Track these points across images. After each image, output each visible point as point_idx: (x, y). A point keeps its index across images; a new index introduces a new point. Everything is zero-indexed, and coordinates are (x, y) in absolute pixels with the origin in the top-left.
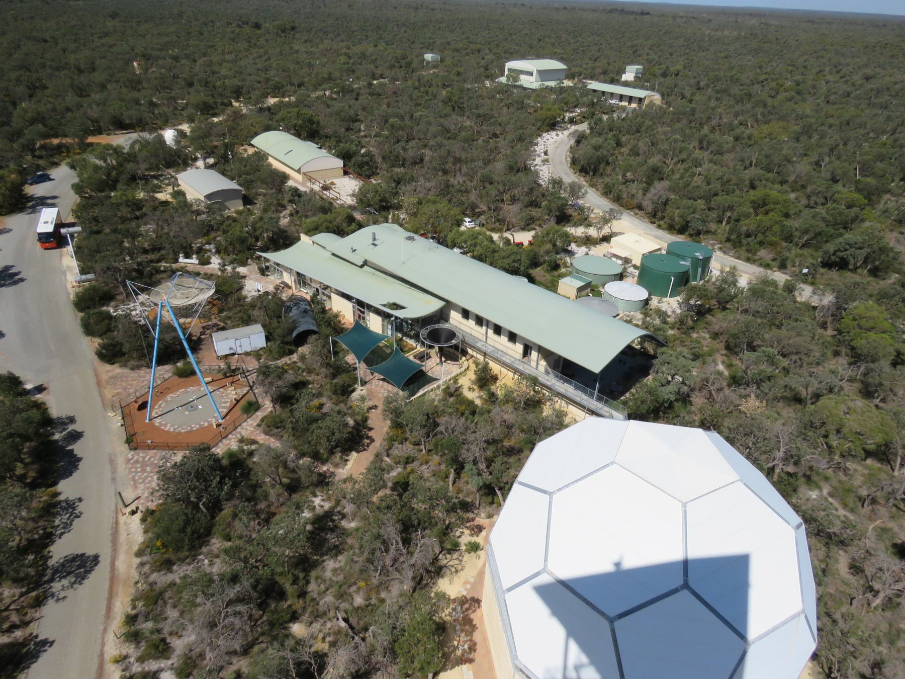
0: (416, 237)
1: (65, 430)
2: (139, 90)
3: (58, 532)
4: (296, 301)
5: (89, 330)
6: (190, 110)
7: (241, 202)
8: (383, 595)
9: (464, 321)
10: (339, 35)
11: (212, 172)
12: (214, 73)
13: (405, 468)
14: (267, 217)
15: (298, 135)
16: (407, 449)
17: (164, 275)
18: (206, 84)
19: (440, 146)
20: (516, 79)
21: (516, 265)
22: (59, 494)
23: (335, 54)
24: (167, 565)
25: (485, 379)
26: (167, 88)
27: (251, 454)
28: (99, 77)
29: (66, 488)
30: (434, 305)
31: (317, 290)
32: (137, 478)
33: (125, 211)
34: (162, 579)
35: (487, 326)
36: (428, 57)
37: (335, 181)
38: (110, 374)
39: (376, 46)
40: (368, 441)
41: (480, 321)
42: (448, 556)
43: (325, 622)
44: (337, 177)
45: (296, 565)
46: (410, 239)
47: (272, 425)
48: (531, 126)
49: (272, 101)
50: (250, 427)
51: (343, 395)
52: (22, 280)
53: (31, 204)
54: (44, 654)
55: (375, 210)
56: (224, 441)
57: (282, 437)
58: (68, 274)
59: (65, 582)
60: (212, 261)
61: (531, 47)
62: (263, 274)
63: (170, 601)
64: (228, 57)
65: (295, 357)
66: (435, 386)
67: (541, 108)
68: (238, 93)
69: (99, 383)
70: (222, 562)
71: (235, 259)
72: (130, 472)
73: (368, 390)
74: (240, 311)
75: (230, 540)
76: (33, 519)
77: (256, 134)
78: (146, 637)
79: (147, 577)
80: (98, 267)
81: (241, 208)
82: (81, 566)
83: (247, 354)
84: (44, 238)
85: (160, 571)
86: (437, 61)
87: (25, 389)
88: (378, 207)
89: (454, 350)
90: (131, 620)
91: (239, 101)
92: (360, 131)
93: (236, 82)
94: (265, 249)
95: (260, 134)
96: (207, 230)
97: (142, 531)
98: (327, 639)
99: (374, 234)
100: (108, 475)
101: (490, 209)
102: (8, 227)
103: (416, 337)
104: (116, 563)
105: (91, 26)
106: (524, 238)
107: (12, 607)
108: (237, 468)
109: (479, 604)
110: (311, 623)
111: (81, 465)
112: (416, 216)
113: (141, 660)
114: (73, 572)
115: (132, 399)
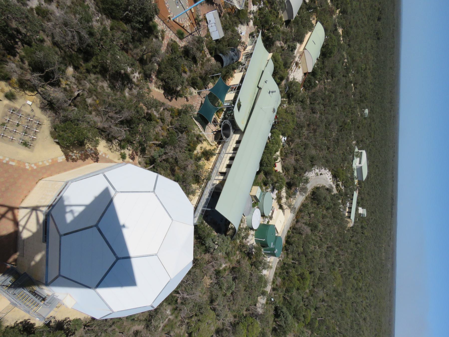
0: (275, 113)
4: (238, 54)
7: (287, 19)
9: (235, 142)
10: (376, 64)
13: (159, 118)
14: (280, 35)
15: (323, 47)
16: (168, 119)
19: (322, 121)
20: (357, 156)
21: (265, 165)
25: (207, 155)
27: (157, 37)
30: (241, 126)
35: (233, 153)
36: (367, 111)
37: (301, 69)
41: (236, 149)
43: (76, 84)
44: (303, 69)
46: (274, 110)
49: (340, 31)
50: (170, 35)
51: (192, 83)
56: (162, 22)
57: (167, 53)
60: (255, 6)
61: (373, 162)
62: (250, 35)
65: (209, 56)
66: (201, 130)
67: (343, 170)
68: (343, 12)
71: (256, 19)
73: (195, 96)
74: (230, 24)
77: (323, 24)
81: (284, 20)
83: (208, 30)
86: (365, 116)
88: (289, 92)
89: (220, 138)
91: (339, 13)
92: (327, 79)
93: (349, 10)
94: (263, 35)
98: (67, 86)
99: (275, 92)
103: (225, 118)
106: (279, 167)
108: (149, 30)
110: (74, 77)
112: (285, 112)
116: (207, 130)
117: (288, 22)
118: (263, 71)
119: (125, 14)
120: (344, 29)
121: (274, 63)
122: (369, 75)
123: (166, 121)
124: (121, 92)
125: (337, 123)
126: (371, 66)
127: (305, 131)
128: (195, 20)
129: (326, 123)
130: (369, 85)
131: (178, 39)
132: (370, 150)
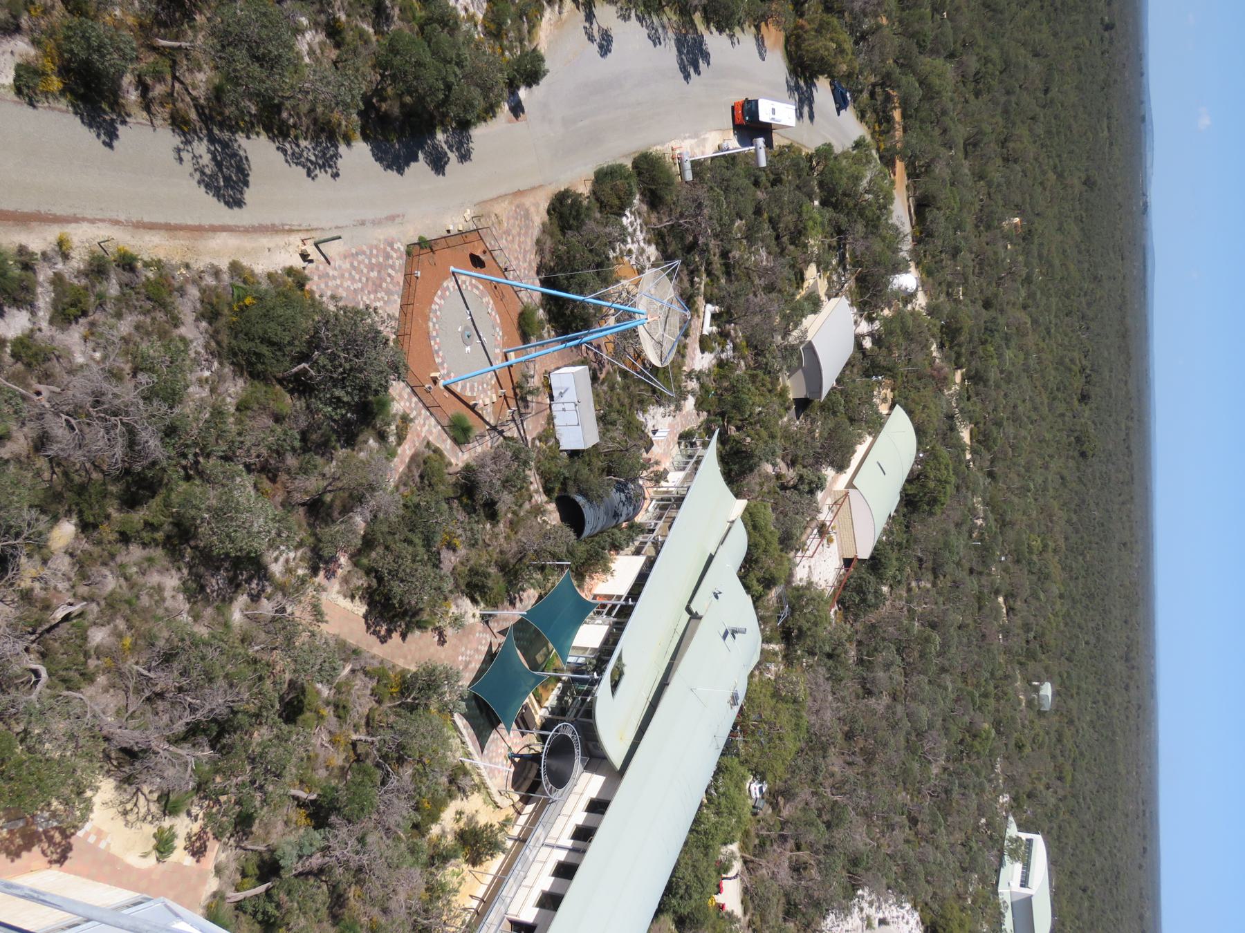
0: (736, 709)
1: (450, 147)
2: (977, 226)
3: (288, 146)
4: (635, 502)
5: (604, 176)
6: (947, 307)
7: (802, 394)
8: (102, 680)
9: (584, 803)
10: (1077, 532)
11: (848, 350)
12: (1007, 338)
13: (328, 704)
14: (772, 440)
15: (913, 479)
16: (362, 704)
17: (686, 284)
18: (990, 331)
19: (894, 726)
20: (1014, 855)
21: (681, 892)
22: (348, 144)
23: (1043, 528)
24: (210, 313)
25: (475, 843)
26: (981, 269)
27: (382, 437)
28: (996, 172)
29: (357, 155)
30: (615, 750)
31: (652, 531)
32: (360, 258)
33: (789, 219)
34: (187, 307)
35: (573, 850)
36: (1047, 690)
37: (834, 545)
38: (532, 209)
39: (1061, 596)
40: (383, 633)
41: (584, 834)
42: (155, 796)
43: (69, 579)
44: (841, 548)
45: (177, 524)
46: (734, 698)
47: (426, 468)
48: (930, 890)
49: (965, 435)
50: (427, 430)
51: (468, 585)
52: (687, 77)
53: (802, 83)
54: (94, 135)
55: (786, 621)
56: (408, 390)
57: (405, 485)
58: (693, 141)
59: (206, 159)
60: (707, 354)
61: (1072, 874)
62: (682, 437)
63: (148, 320)
64: (1032, 361)
65: (540, 498)
66: (471, 749)
67: (963, 909)
68: (975, 378)
69: (519, 193)
70: (202, 399)
71: (707, 392)
72: (371, 248)
73: (472, 626)
74: (622, 405)
75: (238, 409)
76: (312, 110)
77: (910, 413)
78: (94, 286)
79: (194, 282)
80: (701, 192)
81: (791, 396)
82: (228, 182)
83: (551, 419)
84: (750, 108)
85: (202, 301)
86: (1040, 705)
87: (518, 88)
88: (791, 627)
89: (535, 779)
90: (127, 263)
91: (963, 380)
92: (918, 580)
93: (993, 375)
94: (723, 440)
95: (912, 420)
96: (757, 348)
97: (271, 270)
98: (37, 585)
99: (744, 632)
100: (369, 215)
101: (784, 824)
102: (768, 56)
103: (560, 711)
104: (224, 234)
105: (1071, 152)
106: (730, 896)
107: (177, 85)
108: (366, 414)
109: (57, 862)
110: (72, 555)
111: (392, 174)
112: (773, 696)
113: (58, 280)
114: (221, 170)
115: (490, 243)
116: (493, 747)
117: (803, 405)
118: (711, 558)
119: (295, 369)
120: (976, 424)
121: (748, 533)
122: (1055, 569)
123: (353, 713)
124: (218, 608)
125: (946, 730)
126: (1062, 543)
127: (834, 763)
128: (514, 389)
129: (908, 734)
130: (1054, 603)
131: (449, 441)
132: (1060, 827)
